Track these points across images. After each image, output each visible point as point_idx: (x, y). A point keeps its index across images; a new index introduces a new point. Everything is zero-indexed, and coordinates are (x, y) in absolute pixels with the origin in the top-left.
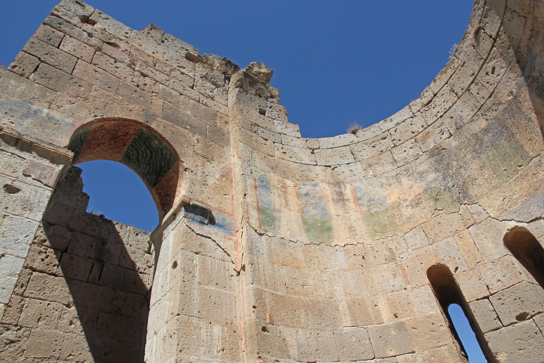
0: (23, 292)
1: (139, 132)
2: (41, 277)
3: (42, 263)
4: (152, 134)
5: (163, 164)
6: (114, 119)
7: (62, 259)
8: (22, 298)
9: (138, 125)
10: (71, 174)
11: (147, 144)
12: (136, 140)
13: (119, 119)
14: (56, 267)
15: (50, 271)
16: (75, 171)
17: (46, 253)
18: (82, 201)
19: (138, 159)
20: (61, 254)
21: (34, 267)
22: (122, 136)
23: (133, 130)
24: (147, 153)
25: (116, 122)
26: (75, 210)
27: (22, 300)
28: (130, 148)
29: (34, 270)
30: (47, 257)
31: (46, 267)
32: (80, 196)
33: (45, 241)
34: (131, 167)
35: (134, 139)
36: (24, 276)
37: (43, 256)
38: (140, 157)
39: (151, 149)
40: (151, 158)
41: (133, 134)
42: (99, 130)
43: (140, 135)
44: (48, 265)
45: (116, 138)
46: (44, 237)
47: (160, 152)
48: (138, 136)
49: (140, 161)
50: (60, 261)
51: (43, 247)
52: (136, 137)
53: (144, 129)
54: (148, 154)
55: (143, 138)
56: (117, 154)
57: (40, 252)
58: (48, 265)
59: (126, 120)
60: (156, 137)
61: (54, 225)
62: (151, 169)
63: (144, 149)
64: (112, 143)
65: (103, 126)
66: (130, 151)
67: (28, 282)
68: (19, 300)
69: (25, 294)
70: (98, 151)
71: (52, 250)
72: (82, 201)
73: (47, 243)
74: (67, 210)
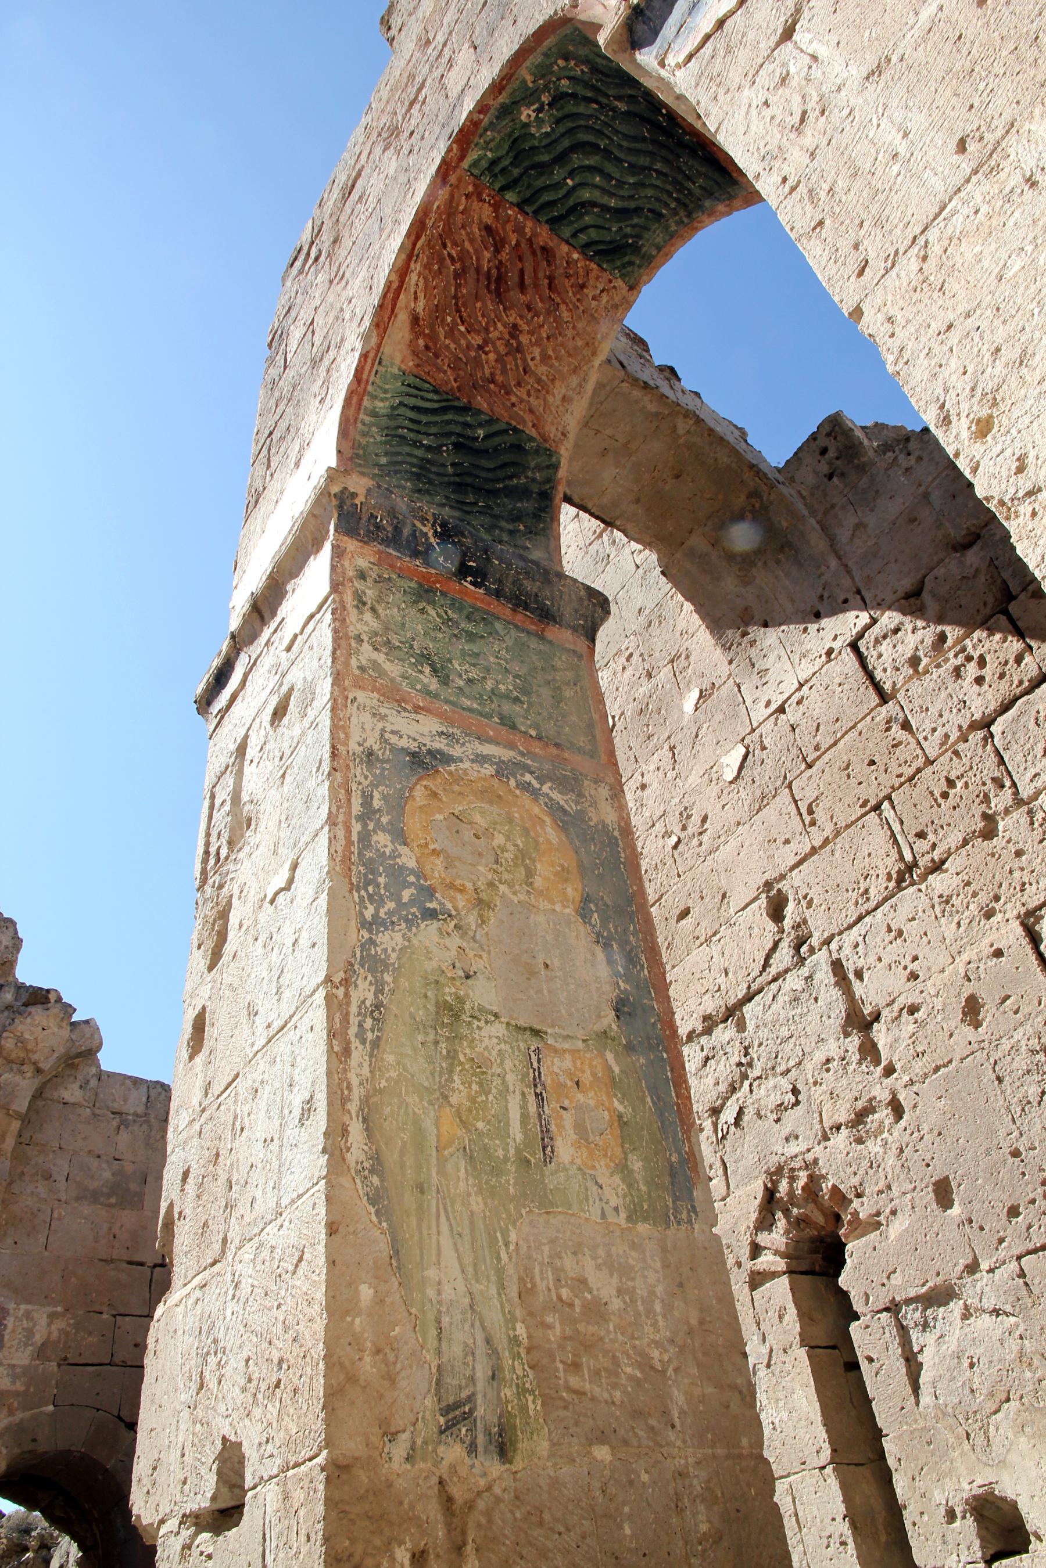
0: (1016, 793)
1: (486, 179)
2: (1016, 720)
3: (985, 687)
4: (491, 126)
5: (622, 106)
6: (402, 272)
7: (1020, 624)
8: (1025, 809)
10: (831, 454)
11: (545, 158)
13: (409, 253)
14: (1028, 659)
15: (1021, 682)
16: (828, 435)
17: (969, 659)
18: (920, 459)
19: (622, 213)
20: (1003, 618)
21: (977, 716)
22: (497, 251)
23: (476, 205)
24: (590, 169)
25: (416, 267)
26: (926, 496)
27: (1030, 812)
28: (567, 232)
29: (986, 723)
30: (982, 662)
31: (1004, 685)
32: (902, 457)
33: (942, 638)
34: (662, 252)
35: (520, 206)
36: (977, 759)
37: (972, 670)
38: (613, 203)
39: (566, 143)
40: (607, 153)
41: (496, 207)
42: (433, 337)
44: (1002, 676)
45: (500, 279)
46: (928, 634)
47: (571, 108)
48: (504, 189)
49: (632, 205)
50: (1021, 635)
51: (951, 654)
52: (511, 196)
53: (473, 155)
54: (591, 161)
55: (516, 172)
56: (590, 292)
57: (957, 672)
58: (1002, 676)
59: (418, 227)
60: (507, 111)
61: (922, 583)
62: (658, 166)
63: (571, 174)
64: (523, 299)
65: (415, 320)
66: (583, 238)
67: (1002, 761)
68: (1025, 820)
69: (1024, 794)
70: (545, 358)
71: (977, 634)
72: (920, 459)
73: (952, 632)
74: (913, 520)
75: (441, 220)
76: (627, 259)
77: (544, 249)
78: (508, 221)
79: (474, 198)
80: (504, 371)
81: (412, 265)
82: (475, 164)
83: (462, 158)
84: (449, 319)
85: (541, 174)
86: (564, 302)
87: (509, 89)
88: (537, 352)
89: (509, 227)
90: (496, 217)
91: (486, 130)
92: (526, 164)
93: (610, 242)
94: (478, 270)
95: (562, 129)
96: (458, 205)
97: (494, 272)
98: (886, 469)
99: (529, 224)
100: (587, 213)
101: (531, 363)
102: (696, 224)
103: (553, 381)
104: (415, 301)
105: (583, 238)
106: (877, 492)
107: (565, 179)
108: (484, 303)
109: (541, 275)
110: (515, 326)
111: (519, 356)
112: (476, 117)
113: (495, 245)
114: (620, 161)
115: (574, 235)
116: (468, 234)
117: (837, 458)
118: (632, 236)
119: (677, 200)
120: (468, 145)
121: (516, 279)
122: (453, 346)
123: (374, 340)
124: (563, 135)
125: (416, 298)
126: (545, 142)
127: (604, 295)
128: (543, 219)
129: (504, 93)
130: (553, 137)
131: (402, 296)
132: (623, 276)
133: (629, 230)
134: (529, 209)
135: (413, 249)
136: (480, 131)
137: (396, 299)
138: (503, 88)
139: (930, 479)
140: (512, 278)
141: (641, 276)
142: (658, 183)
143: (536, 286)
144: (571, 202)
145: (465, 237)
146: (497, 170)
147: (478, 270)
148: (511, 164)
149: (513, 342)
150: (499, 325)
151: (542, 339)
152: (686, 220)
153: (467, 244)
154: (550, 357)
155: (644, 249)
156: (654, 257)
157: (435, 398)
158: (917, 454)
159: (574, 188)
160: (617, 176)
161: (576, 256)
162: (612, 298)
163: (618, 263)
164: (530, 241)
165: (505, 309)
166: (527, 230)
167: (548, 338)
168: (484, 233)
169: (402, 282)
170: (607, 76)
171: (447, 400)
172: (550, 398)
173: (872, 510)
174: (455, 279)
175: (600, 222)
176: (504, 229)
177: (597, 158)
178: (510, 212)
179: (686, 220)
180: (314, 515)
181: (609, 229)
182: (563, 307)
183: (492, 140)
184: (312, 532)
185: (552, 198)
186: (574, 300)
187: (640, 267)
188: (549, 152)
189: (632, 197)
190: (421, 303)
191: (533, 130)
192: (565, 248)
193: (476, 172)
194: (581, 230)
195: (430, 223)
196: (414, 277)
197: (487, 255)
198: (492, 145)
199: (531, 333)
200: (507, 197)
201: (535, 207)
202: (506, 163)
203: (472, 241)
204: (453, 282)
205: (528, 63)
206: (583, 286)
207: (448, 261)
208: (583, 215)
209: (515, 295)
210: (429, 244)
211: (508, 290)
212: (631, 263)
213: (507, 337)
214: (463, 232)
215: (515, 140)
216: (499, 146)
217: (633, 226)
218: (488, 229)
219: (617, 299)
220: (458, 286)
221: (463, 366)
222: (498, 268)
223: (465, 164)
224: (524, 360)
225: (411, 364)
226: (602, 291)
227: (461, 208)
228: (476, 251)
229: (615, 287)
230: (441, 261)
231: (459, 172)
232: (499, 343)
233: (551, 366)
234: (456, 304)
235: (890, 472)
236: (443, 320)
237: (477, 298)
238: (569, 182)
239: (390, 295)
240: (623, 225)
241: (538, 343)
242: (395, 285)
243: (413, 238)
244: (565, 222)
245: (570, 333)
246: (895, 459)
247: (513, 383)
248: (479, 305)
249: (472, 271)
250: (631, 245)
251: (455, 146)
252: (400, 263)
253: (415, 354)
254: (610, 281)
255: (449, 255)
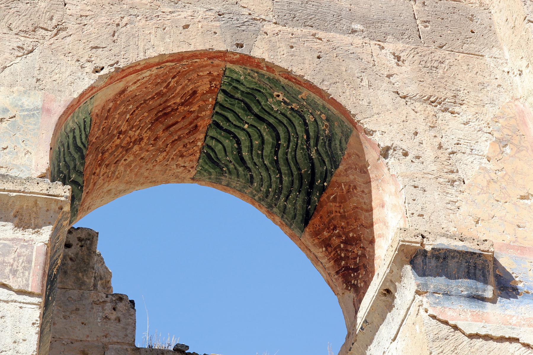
6: (148, 65)
9: (216, 62)
12: (222, 106)
13: (161, 61)
16: (80, 240)
22: (182, 104)
23: (206, 80)
25: (154, 71)
35: (217, 103)
38: (245, 154)
39: (271, 120)
41: (210, 91)
42: (116, 108)
43: (229, 89)
47: (297, 122)
48: (224, 91)
49: (250, 165)
52: (221, 97)
53: (237, 68)
54: (267, 137)
55: (238, 95)
56: (181, 161)
59: (179, 58)
64: (160, 133)
65: (123, 92)
66: (213, 143)
72: (119, 320)
75: (189, 67)
76: (212, 170)
77: (196, 126)
78: (204, 101)
79: (210, 78)
80: (111, 154)
81: (154, 68)
82: (231, 71)
83: (232, 62)
84: (131, 107)
85: (243, 109)
86: (168, 153)
87: (290, 83)
88: (132, 158)
89: (201, 103)
90: (204, 94)
91: (257, 73)
92: (247, 100)
93: (217, 158)
94: (166, 101)
95: (280, 117)
96: (202, 71)
97: (169, 109)
98: (94, 303)
99: (208, 113)
100: (231, 141)
101: (123, 161)
102: (257, 204)
103: (117, 178)
104: (132, 85)
105: (213, 143)
106: (78, 309)
107: (246, 123)
108: (148, 116)
109: (179, 133)
110: (141, 139)
111: (124, 153)
112: (263, 65)
113: (186, 101)
114: (276, 153)
115: (212, 138)
116: (186, 85)
117: (71, 259)
118: (228, 169)
119: (268, 192)
120: (243, 64)
121: (170, 123)
122: (116, 120)
123: (102, 83)
124: (275, 118)
125: (135, 83)
126: (266, 108)
127: (182, 168)
128: (215, 118)
129: (286, 81)
130: (272, 113)
131: (133, 75)
132: (199, 172)
133: (231, 166)
134: (217, 109)
135: (165, 62)
136: (255, 69)
137: (130, 74)
138: (290, 80)
139: (115, 340)
140: (170, 121)
141: (204, 180)
142: (273, 179)
143: (171, 135)
144: (233, 130)
145: (183, 84)
146: (234, 84)
147: (166, 101)
148: (243, 92)
149: (131, 144)
150: (138, 131)
151: (140, 155)
152: (256, 198)
153: (180, 87)
154: (131, 166)
155: (223, 178)
156: (220, 184)
157: (84, 140)
158: (120, 315)
159: (244, 130)
160: (265, 153)
161: (199, 144)
162: (182, 173)
163: (206, 167)
164: (198, 117)
165: (149, 128)
166: (204, 113)
167: (142, 158)
168: (191, 92)
169: (142, 69)
170: (330, 146)
171: (84, 146)
172: (106, 184)
173: (65, 317)
174: (156, 94)
175: (228, 149)
176: (198, 101)
177: (271, 140)
178: (210, 100)
179: (256, 198)
180: (36, 203)
181: (226, 156)
182: (165, 153)
183: (252, 77)
184: (22, 208)
185: (230, 119)
186: (172, 156)
187: (210, 178)
188: (260, 111)
189: (255, 164)
190: (134, 87)
191: (270, 100)
192: (202, 136)
193: (227, 73)
194: (218, 141)
195: (184, 62)
196: (148, 73)
197: (178, 100)
198: (249, 78)
199: (141, 149)
200: (219, 95)
201: (220, 111)
202: (241, 88)
203: (183, 88)
204: (154, 94)
205: (313, 95)
206: (182, 156)
207: (165, 84)
208: (228, 138)
209: (161, 127)
210: (170, 69)
211: (161, 123)
212: (210, 173)
213: (133, 140)
214: (186, 81)
215: (260, 91)
216: (251, 82)
217: (236, 168)
218: (195, 93)
219: (183, 175)
220: (153, 98)
221: (106, 134)
222: (172, 110)
223: (229, 65)
224: (123, 157)
225: (97, 111)
226: (184, 167)
227: (201, 74)
228: (178, 93)
229: (189, 171)
230: (164, 81)
231: (223, 63)
232: (128, 138)
233: (125, 171)
234: (142, 104)
235: (95, 306)
236: (129, 105)
237: (149, 111)
238: (246, 126)
239: (131, 69)
240: (233, 162)
241: (135, 156)
242: (138, 68)
243: (171, 59)
244: (219, 130)
245: (150, 166)
246: (104, 302)
247: (107, 162)
248: (146, 114)
249: (164, 99)
250: (222, 170)
251: (238, 56)
252: (152, 61)
253: (103, 108)
254: (192, 168)
255: (170, 82)
